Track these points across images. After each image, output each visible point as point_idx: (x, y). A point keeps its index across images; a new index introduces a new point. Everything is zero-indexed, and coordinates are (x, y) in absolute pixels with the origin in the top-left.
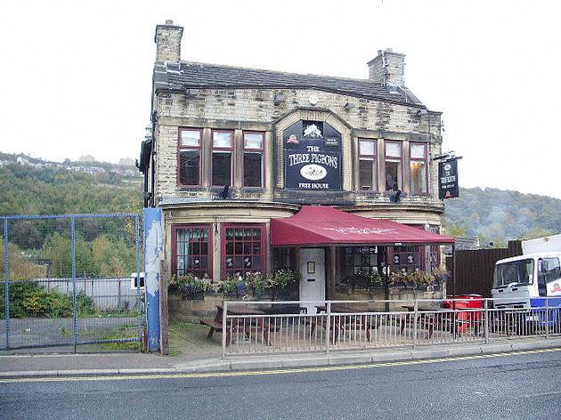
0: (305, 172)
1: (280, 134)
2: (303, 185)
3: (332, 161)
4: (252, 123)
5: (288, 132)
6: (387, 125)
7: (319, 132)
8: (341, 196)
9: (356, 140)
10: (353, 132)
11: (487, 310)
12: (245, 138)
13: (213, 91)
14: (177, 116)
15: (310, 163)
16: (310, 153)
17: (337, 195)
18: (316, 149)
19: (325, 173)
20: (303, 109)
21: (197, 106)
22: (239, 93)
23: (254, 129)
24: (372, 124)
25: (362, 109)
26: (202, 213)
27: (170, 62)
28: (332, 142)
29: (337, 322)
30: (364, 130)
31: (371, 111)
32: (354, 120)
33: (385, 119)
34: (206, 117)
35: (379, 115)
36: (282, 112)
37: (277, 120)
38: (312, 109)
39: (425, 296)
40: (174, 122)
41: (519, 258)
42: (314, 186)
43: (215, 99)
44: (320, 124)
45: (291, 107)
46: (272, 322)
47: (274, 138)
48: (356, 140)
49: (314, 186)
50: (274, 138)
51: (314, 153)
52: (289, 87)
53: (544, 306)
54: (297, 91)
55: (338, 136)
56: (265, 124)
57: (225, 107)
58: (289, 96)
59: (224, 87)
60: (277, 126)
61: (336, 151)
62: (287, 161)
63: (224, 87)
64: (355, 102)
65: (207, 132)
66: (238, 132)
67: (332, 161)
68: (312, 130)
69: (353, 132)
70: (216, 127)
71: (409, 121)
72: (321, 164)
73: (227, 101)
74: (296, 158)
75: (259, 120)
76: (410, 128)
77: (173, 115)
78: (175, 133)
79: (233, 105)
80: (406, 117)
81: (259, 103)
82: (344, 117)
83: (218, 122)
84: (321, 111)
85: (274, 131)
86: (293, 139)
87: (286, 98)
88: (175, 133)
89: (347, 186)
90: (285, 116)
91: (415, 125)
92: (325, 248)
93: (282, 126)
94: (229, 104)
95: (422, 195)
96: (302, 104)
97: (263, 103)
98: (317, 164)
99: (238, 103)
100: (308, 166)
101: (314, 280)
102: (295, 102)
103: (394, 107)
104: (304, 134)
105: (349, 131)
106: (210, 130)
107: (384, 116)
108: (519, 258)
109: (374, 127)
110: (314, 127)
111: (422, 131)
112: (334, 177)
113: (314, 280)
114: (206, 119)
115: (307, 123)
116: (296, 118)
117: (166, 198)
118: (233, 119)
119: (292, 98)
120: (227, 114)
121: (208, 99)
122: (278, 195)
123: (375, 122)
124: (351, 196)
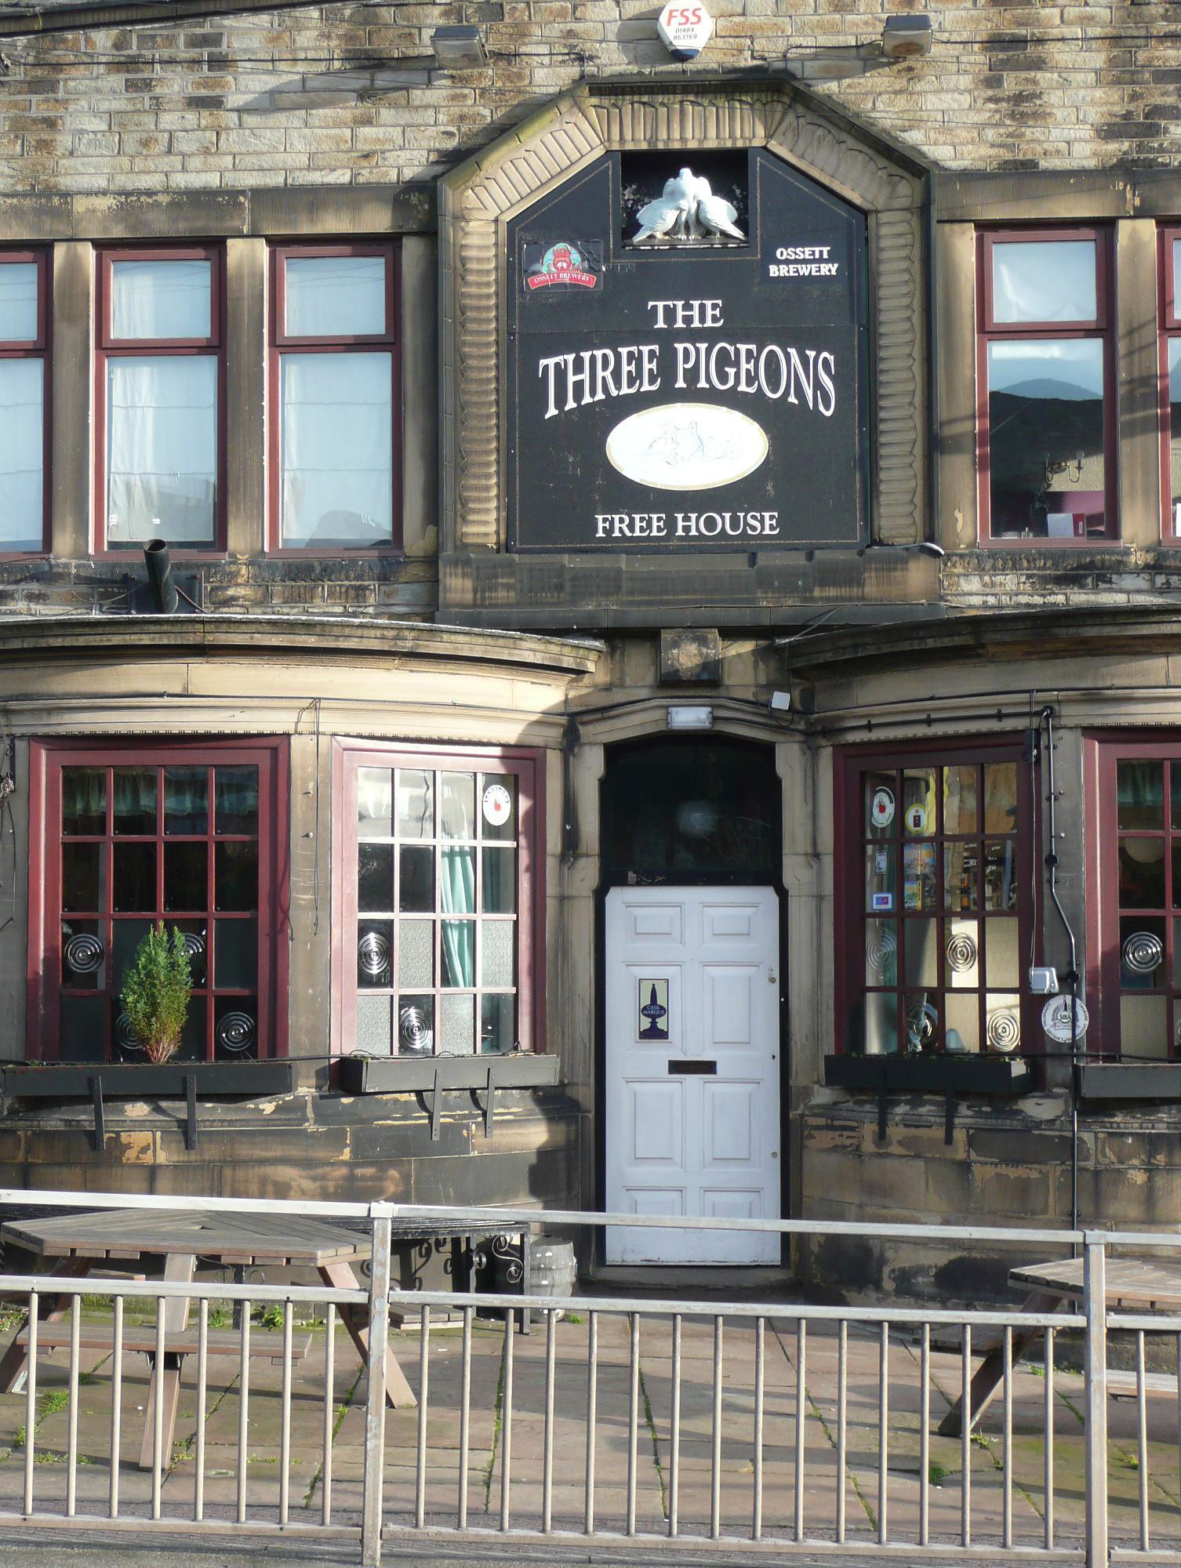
4: (317, 197)
5: (530, 230)
7: (721, 213)
9: (963, 244)
15: (667, 395)
16: (666, 339)
18: (707, 312)
30: (1021, 173)
31: (1059, 54)
34: (65, 182)
41: (1143, 1367)
42: (692, 524)
44: (726, 169)
48: (963, 244)
49: (692, 524)
51: (694, 336)
53: (222, 904)
57: (169, 120)
62: (523, 391)
65: (74, 263)
73: (176, 84)
74: (581, 375)
75: (366, 176)
79: (213, 103)
83: (131, 200)
86: (561, 265)
92: (272, 748)
98: (711, 396)
101: (708, 1067)
104: (634, 227)
105: (906, 191)
106: (89, 254)
108: (1143, 1367)
109: (1086, 152)
110: (693, 189)
113: (708, 1067)
114: (66, 195)
115: (648, 171)
116: (564, 147)
121: (75, 81)
123: (1094, 115)
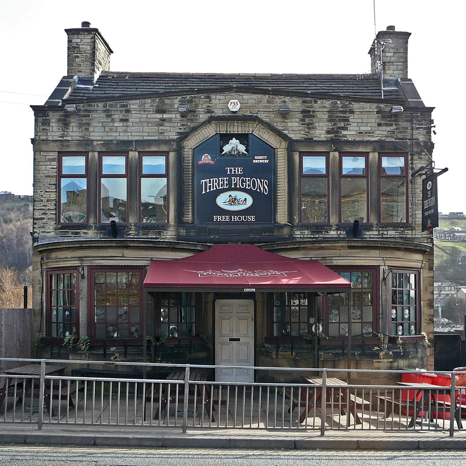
0: (222, 201)
1: (188, 153)
2: (219, 218)
3: (262, 186)
6: (344, 132)
7: (242, 148)
8: (271, 230)
10: (292, 146)
11: (188, 381)
12: (342, 182)
13: (101, 105)
14: (55, 138)
16: (230, 176)
17: (266, 230)
18: (239, 170)
19: (250, 201)
20: (220, 119)
21: (80, 125)
22: (134, 105)
23: (153, 149)
24: (321, 132)
25: (307, 114)
26: (69, 254)
27: (82, 75)
28: (260, 159)
29: (200, 394)
30: (309, 141)
31: (319, 115)
32: (294, 129)
33: (342, 124)
34: (92, 138)
35: (331, 119)
36: (192, 125)
37: (184, 136)
38: (234, 118)
39: (376, 365)
40: (53, 146)
43: (103, 115)
44: (243, 138)
45: (203, 117)
46: (56, 388)
47: (180, 159)
48: (296, 157)
50: (180, 159)
51: (236, 176)
52: (200, 91)
54: (213, 96)
55: (270, 152)
56: (167, 142)
57: (116, 124)
58: (202, 104)
59: (113, 98)
60: (185, 143)
61: (269, 172)
63: (113, 98)
64: (295, 104)
66: (133, 155)
67: (262, 186)
68: (234, 145)
69: (292, 146)
70: (104, 150)
71: (379, 125)
72: (245, 190)
74: (210, 184)
75: (161, 138)
76: (381, 133)
77: (50, 138)
78: (53, 160)
79: (127, 120)
80: (374, 119)
81: (159, 116)
82: (279, 127)
83: (107, 143)
84: (245, 119)
85: (179, 151)
86: (206, 159)
87: (197, 106)
88: (53, 160)
89: (282, 217)
90: (194, 129)
91: (389, 128)
93: (191, 143)
94: (122, 120)
95: (396, 226)
96: (218, 113)
97: (165, 116)
99: (134, 118)
100: (227, 194)
101: (238, 340)
102: (209, 111)
103: (356, 106)
106: (96, 154)
107: (339, 119)
109: (323, 137)
111: (400, 136)
112: (264, 204)
113: (238, 340)
114: (92, 141)
115: (226, 138)
116: (210, 131)
117: (44, 238)
118: (125, 138)
119: (205, 106)
120: (119, 134)
122: (183, 232)
123: (325, 128)
124: (286, 231)
